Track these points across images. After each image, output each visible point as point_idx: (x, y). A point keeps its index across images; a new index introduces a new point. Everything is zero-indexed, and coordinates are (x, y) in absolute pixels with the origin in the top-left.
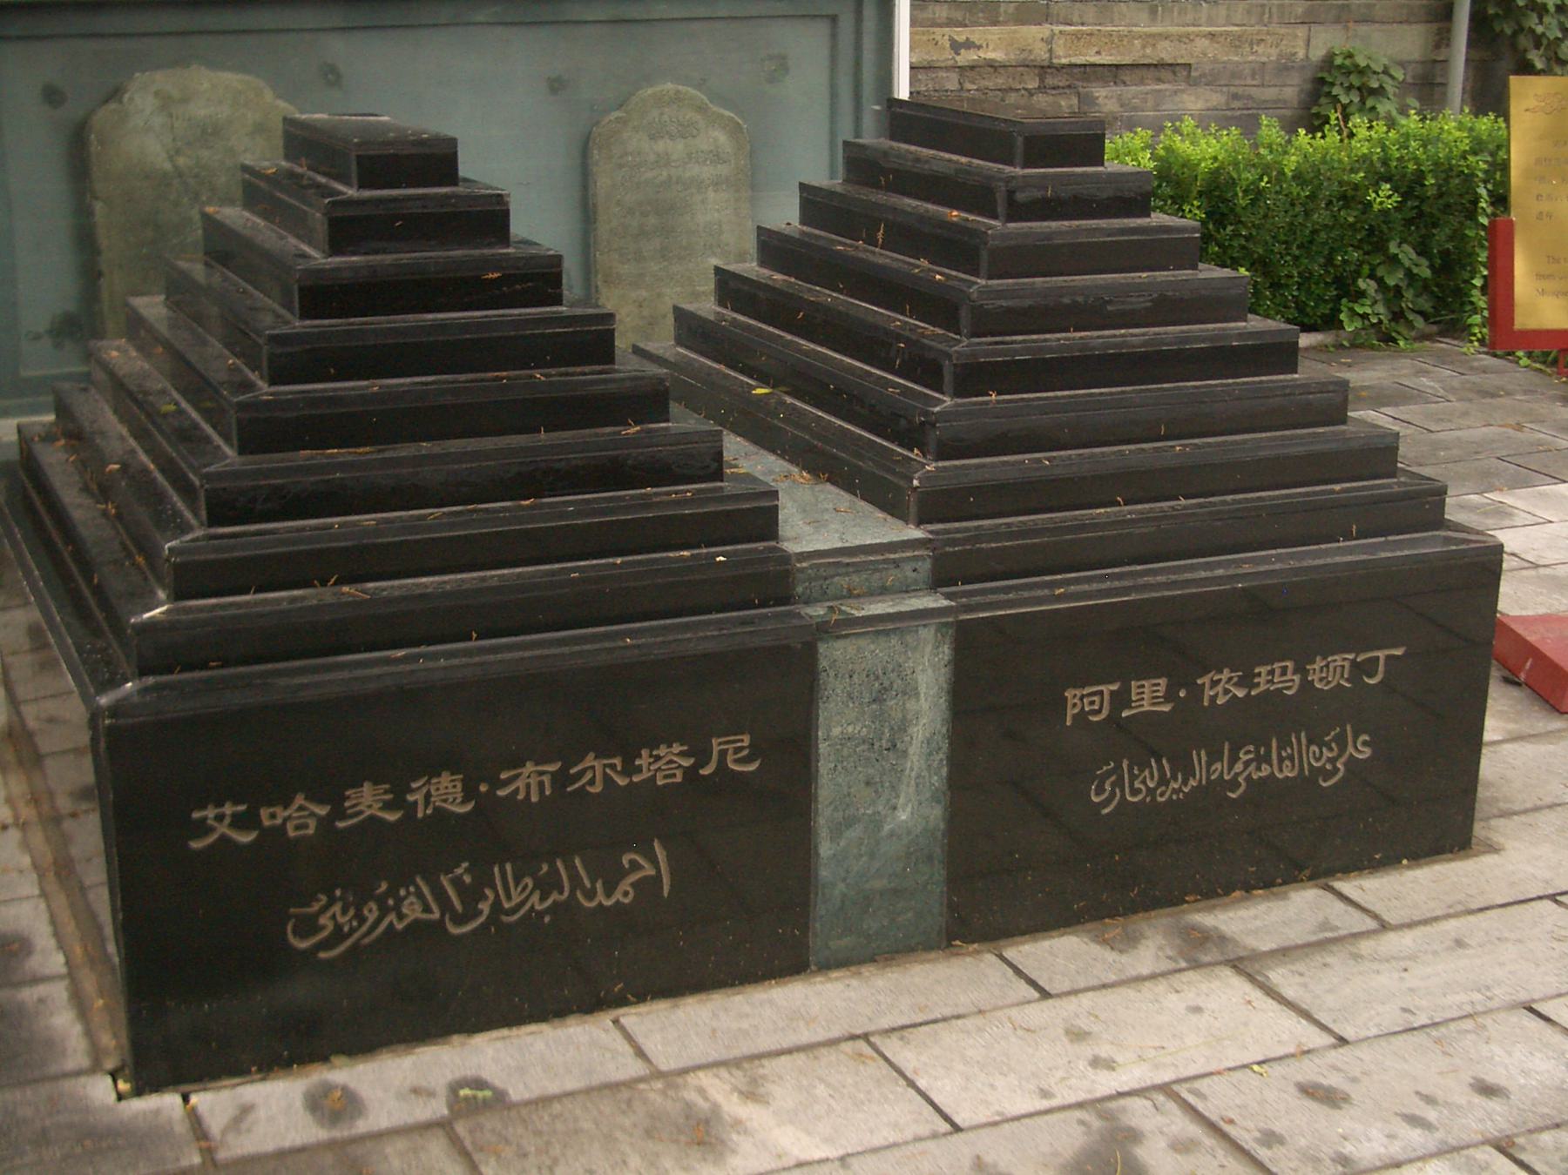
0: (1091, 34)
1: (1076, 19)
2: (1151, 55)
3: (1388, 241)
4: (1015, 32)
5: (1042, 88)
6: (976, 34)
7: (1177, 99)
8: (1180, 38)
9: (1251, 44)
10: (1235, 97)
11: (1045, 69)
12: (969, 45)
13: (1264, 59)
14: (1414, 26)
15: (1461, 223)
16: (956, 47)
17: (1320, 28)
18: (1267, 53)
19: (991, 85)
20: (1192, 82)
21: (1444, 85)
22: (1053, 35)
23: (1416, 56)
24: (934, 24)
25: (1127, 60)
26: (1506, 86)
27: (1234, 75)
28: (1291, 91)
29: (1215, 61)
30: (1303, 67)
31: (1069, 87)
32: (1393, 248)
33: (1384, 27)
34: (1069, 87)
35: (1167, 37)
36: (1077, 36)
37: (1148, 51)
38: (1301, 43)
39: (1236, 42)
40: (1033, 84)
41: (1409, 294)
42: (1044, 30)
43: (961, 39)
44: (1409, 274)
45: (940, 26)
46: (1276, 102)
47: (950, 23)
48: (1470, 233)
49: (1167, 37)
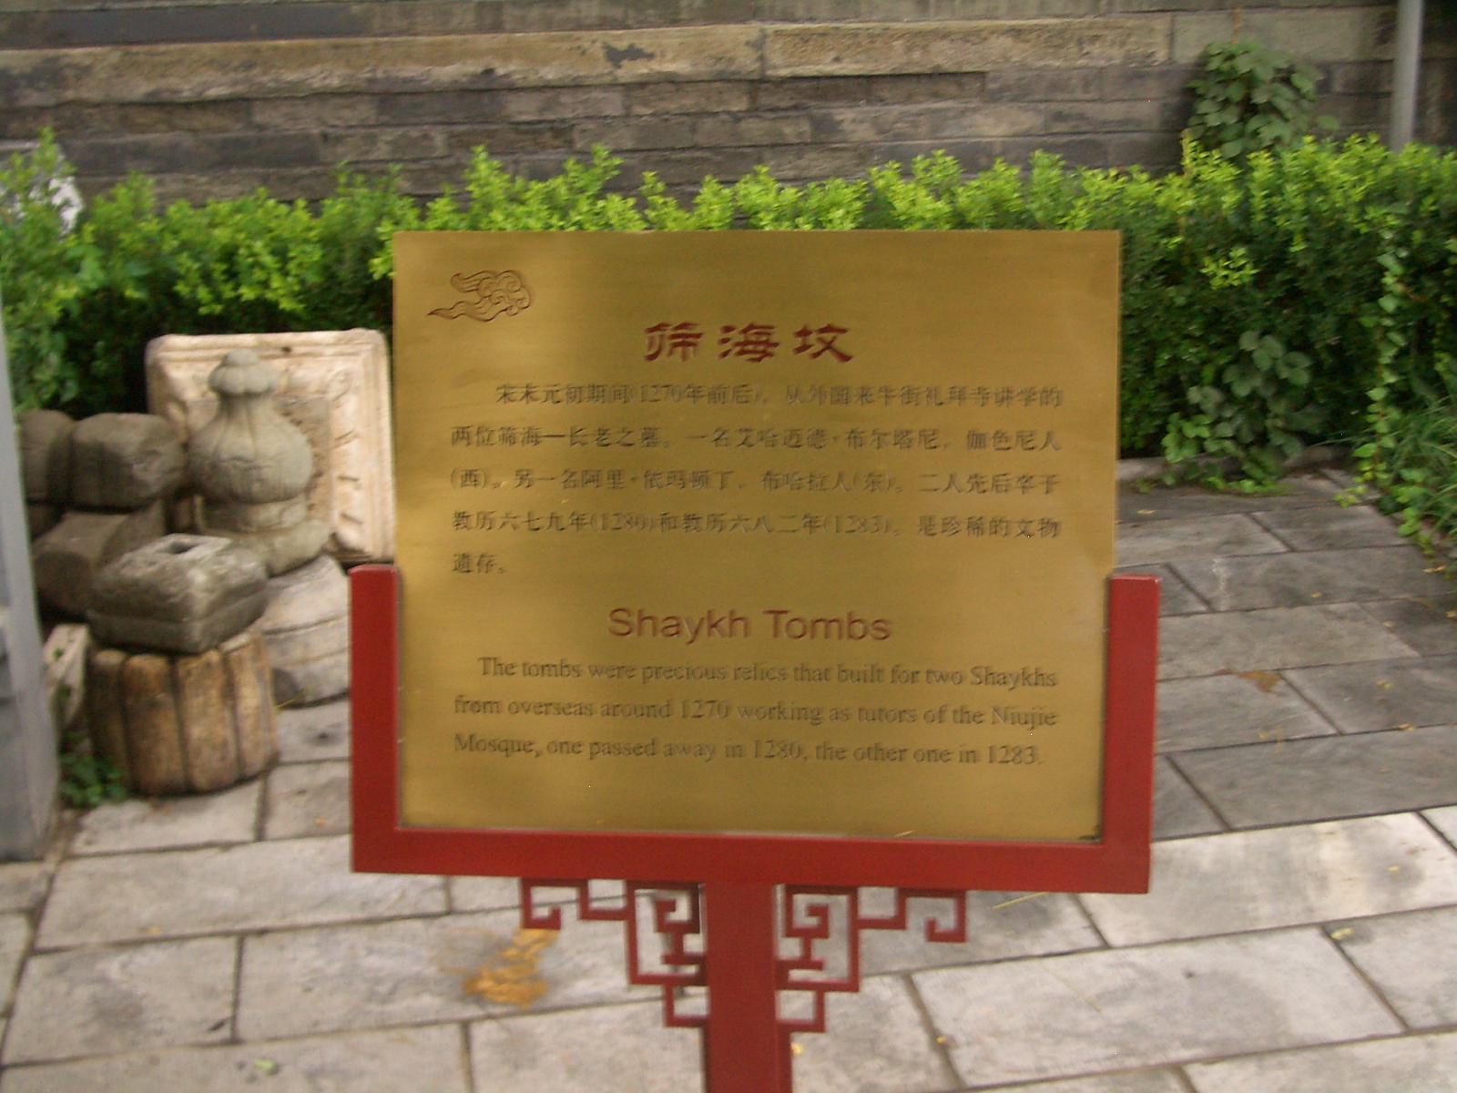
0: (824, 34)
1: (800, 13)
2: (919, 61)
3: (1243, 330)
4: (705, 34)
5: (754, 111)
6: (644, 38)
7: (966, 122)
8: (967, 37)
9: (1080, 42)
10: (1059, 117)
11: (757, 84)
12: (634, 54)
13: (1102, 63)
14: (1342, 13)
15: (1357, 304)
16: (615, 57)
17: (1192, 18)
18: (1105, 54)
19: (672, 106)
20: (993, 98)
21: (1389, 94)
22: (764, 36)
23: (1349, 53)
24: (580, 26)
25: (884, 69)
26: (245, 302)
27: (1055, 86)
28: (1148, 108)
29: (1023, 66)
30: (1163, 75)
31: (795, 107)
32: (1247, 342)
33: (1296, 14)
34: (795, 107)
35: (945, 35)
36: (804, 37)
37: (916, 55)
38: (1160, 39)
39: (1057, 39)
40: (739, 105)
41: (1280, 407)
42: (752, 29)
43: (622, 45)
44: (1272, 377)
45: (589, 28)
46: (1121, 123)
47: (604, 23)
48: (1368, 321)
49: (945, 35)
